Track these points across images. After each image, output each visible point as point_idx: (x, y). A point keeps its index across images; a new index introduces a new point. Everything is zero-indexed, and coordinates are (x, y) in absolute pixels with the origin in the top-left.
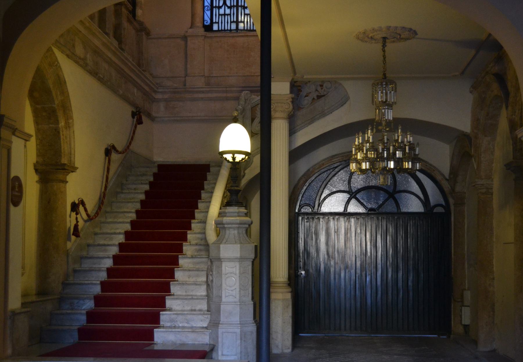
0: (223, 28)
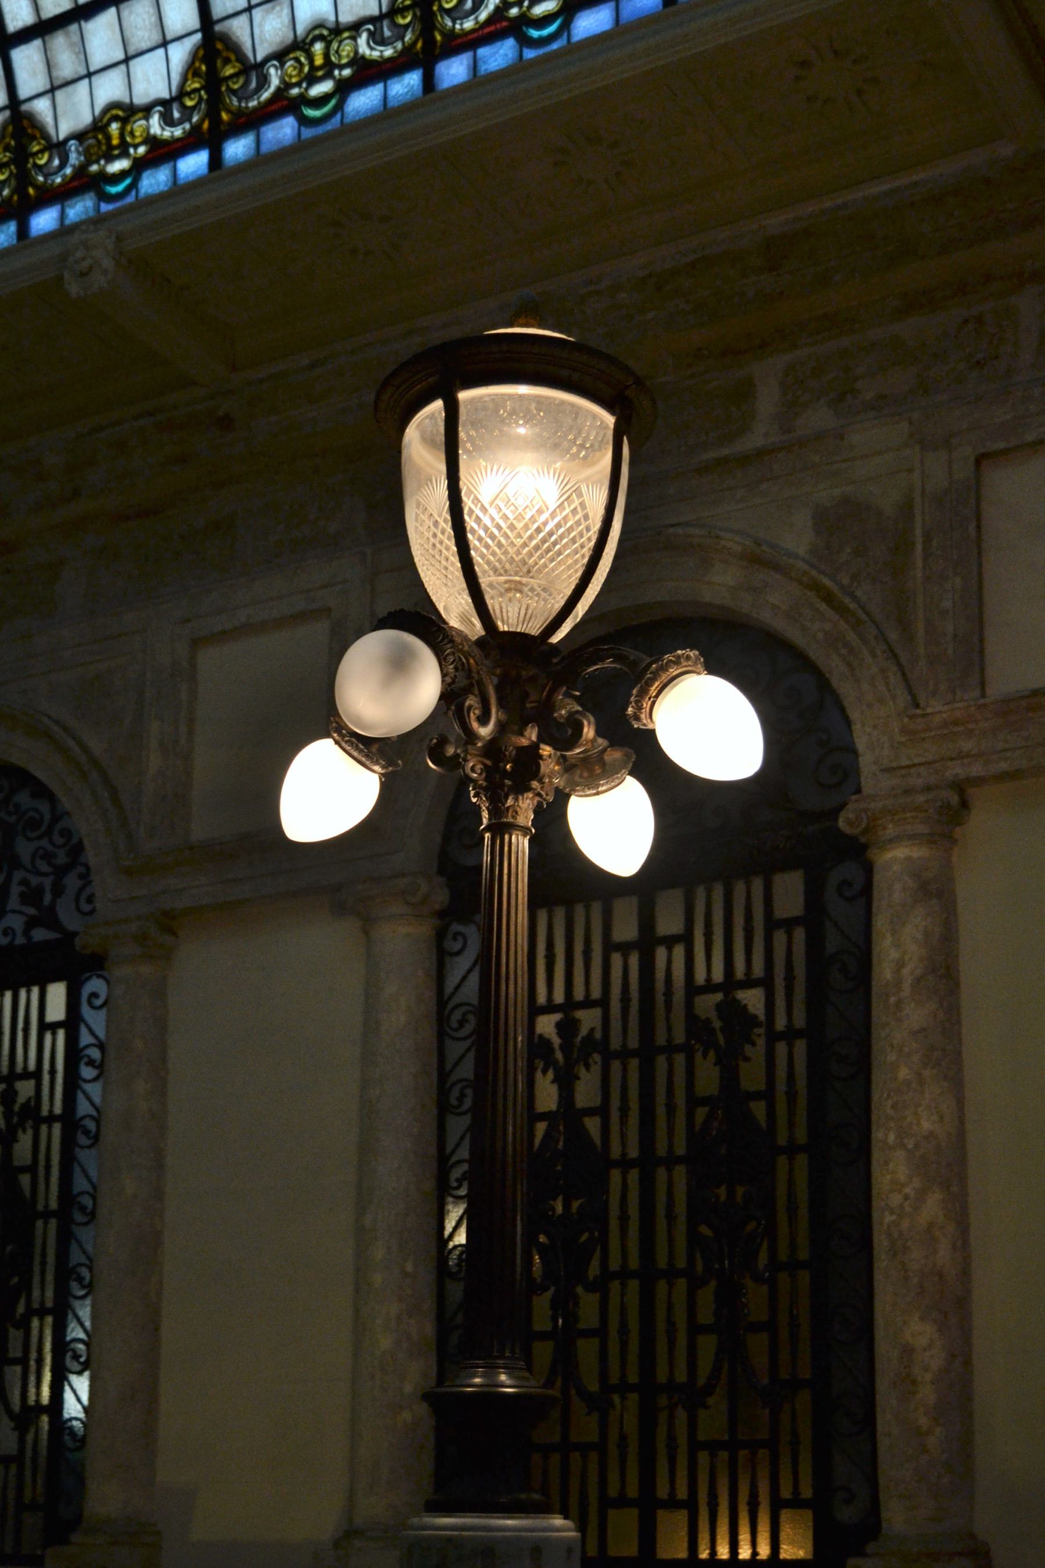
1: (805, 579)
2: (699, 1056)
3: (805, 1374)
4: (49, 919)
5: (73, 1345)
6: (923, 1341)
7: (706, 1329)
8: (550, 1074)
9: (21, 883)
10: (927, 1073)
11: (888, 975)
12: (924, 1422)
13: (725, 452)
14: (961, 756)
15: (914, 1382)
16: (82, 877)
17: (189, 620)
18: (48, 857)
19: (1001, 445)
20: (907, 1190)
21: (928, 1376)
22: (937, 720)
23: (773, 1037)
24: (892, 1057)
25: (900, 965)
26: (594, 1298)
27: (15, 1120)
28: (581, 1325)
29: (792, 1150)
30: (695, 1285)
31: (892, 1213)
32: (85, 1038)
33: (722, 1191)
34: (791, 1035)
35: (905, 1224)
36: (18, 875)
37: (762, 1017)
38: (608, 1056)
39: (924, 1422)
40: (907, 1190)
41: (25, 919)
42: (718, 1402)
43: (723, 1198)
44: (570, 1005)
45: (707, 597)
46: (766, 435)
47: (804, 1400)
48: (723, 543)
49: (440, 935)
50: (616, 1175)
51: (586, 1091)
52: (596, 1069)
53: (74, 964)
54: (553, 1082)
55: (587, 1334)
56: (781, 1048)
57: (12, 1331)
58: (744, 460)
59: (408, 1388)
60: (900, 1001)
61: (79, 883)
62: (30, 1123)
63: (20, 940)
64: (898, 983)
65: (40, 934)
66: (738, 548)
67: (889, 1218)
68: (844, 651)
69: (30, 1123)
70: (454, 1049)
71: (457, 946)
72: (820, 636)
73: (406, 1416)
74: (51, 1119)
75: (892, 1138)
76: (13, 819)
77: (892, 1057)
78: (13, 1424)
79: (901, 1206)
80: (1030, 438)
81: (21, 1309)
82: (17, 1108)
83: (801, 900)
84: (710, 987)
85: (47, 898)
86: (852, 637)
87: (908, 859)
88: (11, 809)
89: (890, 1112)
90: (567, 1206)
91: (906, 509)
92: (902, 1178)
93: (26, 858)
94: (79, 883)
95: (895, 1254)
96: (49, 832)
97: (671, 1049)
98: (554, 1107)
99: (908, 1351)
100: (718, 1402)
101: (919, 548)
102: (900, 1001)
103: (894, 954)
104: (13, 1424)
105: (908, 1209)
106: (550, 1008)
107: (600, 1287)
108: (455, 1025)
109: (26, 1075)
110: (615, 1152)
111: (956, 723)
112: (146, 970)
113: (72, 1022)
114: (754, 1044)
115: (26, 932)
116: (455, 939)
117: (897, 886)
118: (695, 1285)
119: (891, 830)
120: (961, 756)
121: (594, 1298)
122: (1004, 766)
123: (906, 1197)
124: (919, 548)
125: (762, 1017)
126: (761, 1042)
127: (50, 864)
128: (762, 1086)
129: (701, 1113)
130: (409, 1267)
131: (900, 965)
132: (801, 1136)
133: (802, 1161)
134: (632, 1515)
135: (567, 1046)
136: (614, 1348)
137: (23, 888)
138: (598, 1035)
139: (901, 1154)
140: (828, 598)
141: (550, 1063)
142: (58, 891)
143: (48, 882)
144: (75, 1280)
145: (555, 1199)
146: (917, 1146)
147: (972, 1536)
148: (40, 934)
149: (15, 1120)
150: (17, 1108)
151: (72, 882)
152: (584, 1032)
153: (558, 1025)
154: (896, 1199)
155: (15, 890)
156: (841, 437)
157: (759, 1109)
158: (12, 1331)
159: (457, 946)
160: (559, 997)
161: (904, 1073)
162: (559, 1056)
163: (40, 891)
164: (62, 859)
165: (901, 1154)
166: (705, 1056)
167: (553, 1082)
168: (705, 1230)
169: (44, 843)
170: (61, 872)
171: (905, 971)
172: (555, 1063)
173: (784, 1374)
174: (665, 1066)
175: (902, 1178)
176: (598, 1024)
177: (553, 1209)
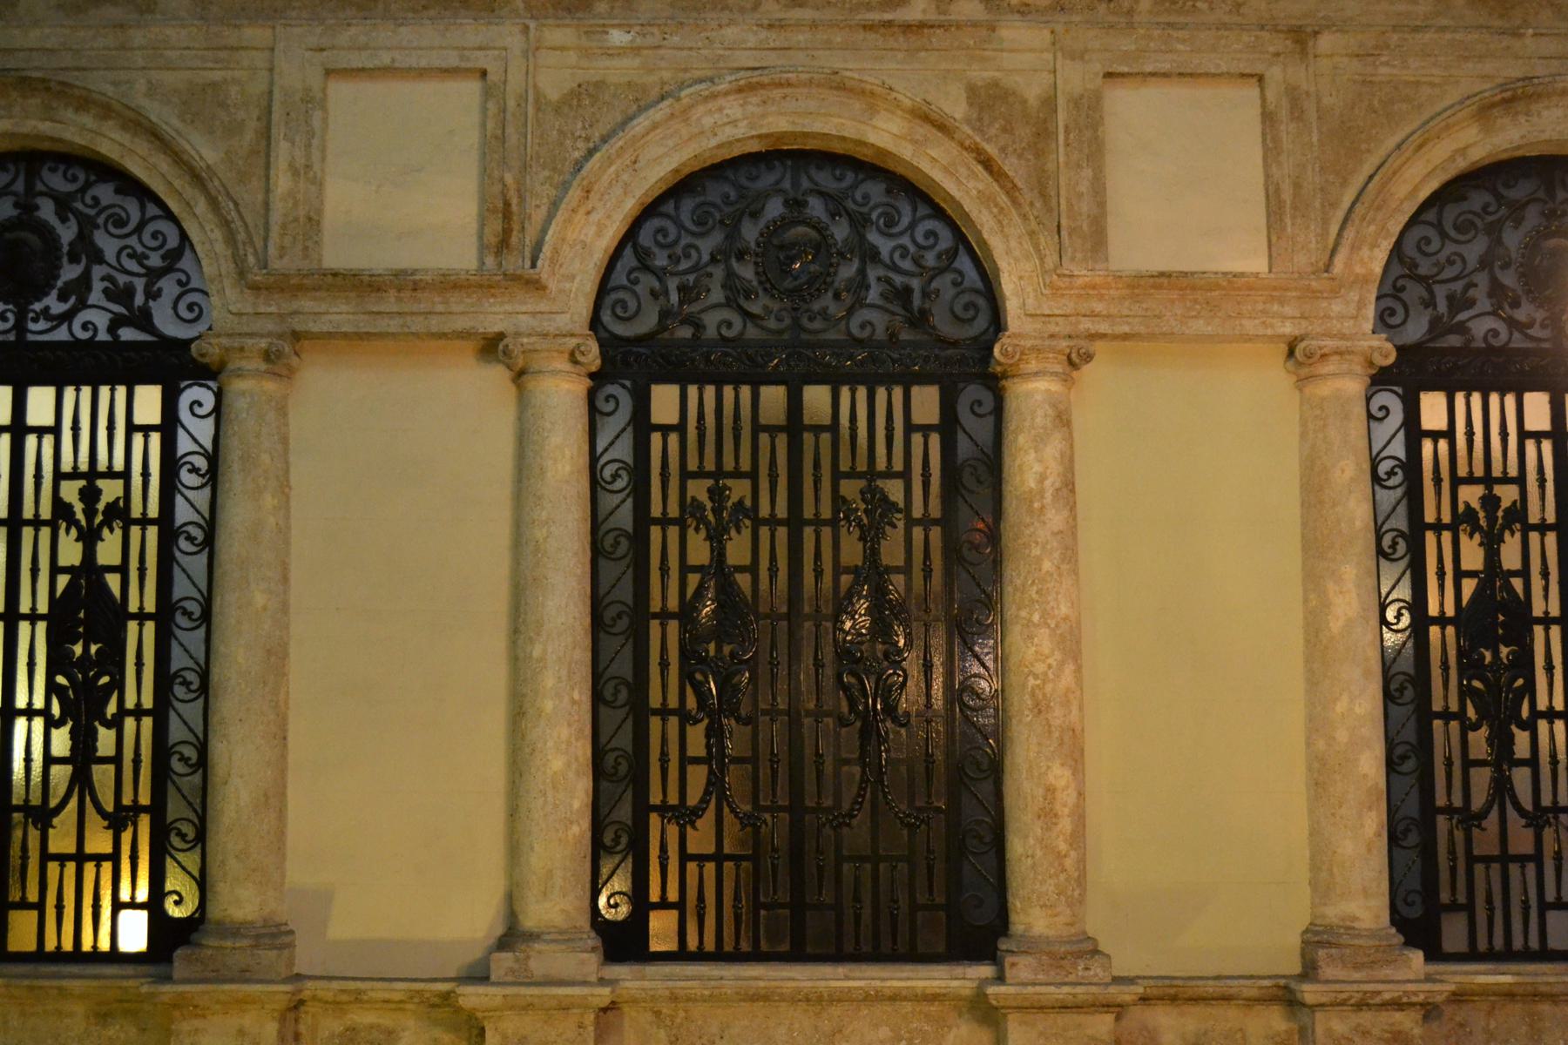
0: (68, 945)
1: (967, 143)
2: (62, 532)
3: (145, 799)
4: (143, 320)
5: (177, 748)
6: (1063, 783)
7: (696, 761)
8: (703, 533)
9: (103, 279)
10: (1064, 567)
11: (1032, 483)
12: (1063, 847)
13: (888, 16)
14: (1093, 315)
15: (1056, 815)
16: (180, 282)
17: (322, 50)
18: (140, 258)
19: (1126, 69)
20: (1050, 661)
21: (1066, 811)
22: (1080, 282)
23: (910, 522)
24: (1036, 551)
25: (1042, 478)
26: (112, 733)
27: (99, 518)
28: (99, 754)
29: (141, 617)
30: (1467, 727)
31: (1036, 677)
32: (184, 444)
33: (712, 647)
34: (926, 522)
35: (1049, 688)
36: (98, 271)
37: (902, 505)
38: (757, 522)
39: (1063, 847)
40: (1050, 661)
41: (110, 315)
42: (706, 822)
43: (712, 653)
44: (719, 473)
45: (873, 138)
46: (924, 11)
47: (144, 822)
48: (894, 95)
49: (591, 396)
50: (132, 626)
51: (108, 551)
52: (747, 533)
53: (173, 365)
54: (77, 540)
55: (104, 760)
56: (918, 532)
57: (102, 731)
58: (907, 28)
59: (576, 804)
60: (1043, 507)
61: (177, 290)
62: (117, 524)
63: (103, 336)
64: (1042, 493)
65: (127, 334)
66: (907, 103)
67: (1032, 682)
68: (995, 210)
69: (117, 524)
70: (608, 501)
71: (610, 407)
72: (974, 192)
73: (575, 829)
74: (144, 522)
75: (1036, 618)
76: (92, 212)
77: (1036, 551)
78: (106, 823)
79: (1045, 674)
80: (1149, 68)
81: (112, 708)
82: (101, 506)
83: (937, 410)
84: (75, 475)
85: (139, 300)
86: (1003, 199)
87: (1048, 391)
88: (88, 200)
89: (1035, 596)
90: (86, 649)
91: (1049, 103)
92: (1047, 651)
93: (110, 256)
94: (177, 290)
95: (1040, 712)
96: (139, 230)
97: (37, 523)
98: (77, 563)
99: (1050, 790)
100: (706, 822)
101: (1061, 137)
102: (1043, 507)
103: (1037, 468)
104: (106, 823)
105: (1051, 676)
106: (701, 474)
107: (116, 723)
108: (609, 479)
109: (110, 474)
110: (133, 607)
111: (1094, 288)
112: (270, 386)
113: (169, 425)
114: (895, 526)
115: (112, 329)
116: (607, 400)
117: (1040, 412)
118: (51, 724)
119: (1033, 366)
120: (1093, 315)
121: (112, 733)
122: (1126, 329)
123: (1050, 666)
124: (1061, 137)
125: (902, 505)
126: (901, 524)
127: (142, 265)
128: (747, 561)
129: (63, 581)
130: (576, 696)
131: (1042, 478)
132: (150, 607)
133: (150, 626)
134: (90, 848)
135: (90, 512)
136: (764, 773)
137: (106, 284)
138: (748, 503)
139: (1044, 631)
140: (987, 164)
141: (72, 521)
142: (153, 294)
143: (140, 284)
144: (181, 684)
145: (74, 643)
146: (1057, 626)
147: (1085, 933)
148: (127, 334)
149: (99, 518)
150: (101, 506)
151: (168, 286)
152: (734, 499)
153: (82, 492)
154: (1040, 668)
155: (98, 286)
156: (993, 30)
157: (113, 581)
158: (102, 731)
159: (610, 407)
160: (710, 466)
161: (1047, 565)
162: (80, 516)
163: (129, 292)
164: (155, 260)
165: (1044, 631)
166: (68, 531)
167: (77, 540)
168: (61, 679)
169: (133, 241)
170: (153, 275)
171: (1048, 483)
172: (77, 523)
173: (1546, 801)
174: (813, 537)
175: (1047, 651)
176: (121, 493)
177: (707, 651)
